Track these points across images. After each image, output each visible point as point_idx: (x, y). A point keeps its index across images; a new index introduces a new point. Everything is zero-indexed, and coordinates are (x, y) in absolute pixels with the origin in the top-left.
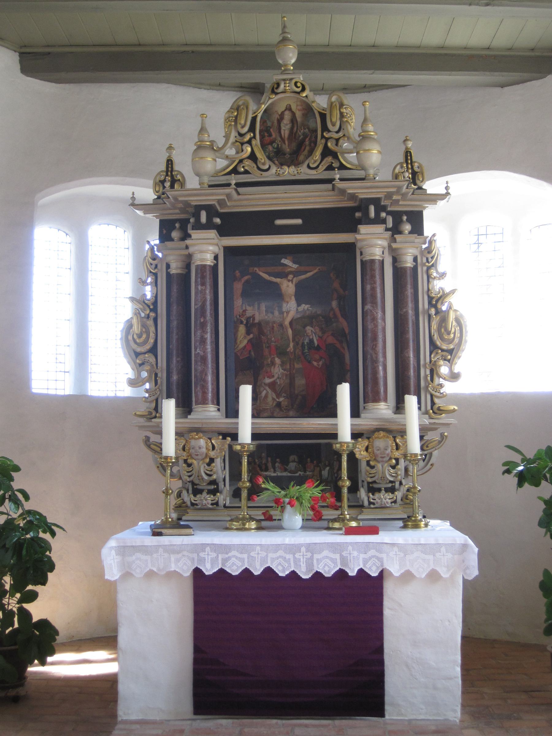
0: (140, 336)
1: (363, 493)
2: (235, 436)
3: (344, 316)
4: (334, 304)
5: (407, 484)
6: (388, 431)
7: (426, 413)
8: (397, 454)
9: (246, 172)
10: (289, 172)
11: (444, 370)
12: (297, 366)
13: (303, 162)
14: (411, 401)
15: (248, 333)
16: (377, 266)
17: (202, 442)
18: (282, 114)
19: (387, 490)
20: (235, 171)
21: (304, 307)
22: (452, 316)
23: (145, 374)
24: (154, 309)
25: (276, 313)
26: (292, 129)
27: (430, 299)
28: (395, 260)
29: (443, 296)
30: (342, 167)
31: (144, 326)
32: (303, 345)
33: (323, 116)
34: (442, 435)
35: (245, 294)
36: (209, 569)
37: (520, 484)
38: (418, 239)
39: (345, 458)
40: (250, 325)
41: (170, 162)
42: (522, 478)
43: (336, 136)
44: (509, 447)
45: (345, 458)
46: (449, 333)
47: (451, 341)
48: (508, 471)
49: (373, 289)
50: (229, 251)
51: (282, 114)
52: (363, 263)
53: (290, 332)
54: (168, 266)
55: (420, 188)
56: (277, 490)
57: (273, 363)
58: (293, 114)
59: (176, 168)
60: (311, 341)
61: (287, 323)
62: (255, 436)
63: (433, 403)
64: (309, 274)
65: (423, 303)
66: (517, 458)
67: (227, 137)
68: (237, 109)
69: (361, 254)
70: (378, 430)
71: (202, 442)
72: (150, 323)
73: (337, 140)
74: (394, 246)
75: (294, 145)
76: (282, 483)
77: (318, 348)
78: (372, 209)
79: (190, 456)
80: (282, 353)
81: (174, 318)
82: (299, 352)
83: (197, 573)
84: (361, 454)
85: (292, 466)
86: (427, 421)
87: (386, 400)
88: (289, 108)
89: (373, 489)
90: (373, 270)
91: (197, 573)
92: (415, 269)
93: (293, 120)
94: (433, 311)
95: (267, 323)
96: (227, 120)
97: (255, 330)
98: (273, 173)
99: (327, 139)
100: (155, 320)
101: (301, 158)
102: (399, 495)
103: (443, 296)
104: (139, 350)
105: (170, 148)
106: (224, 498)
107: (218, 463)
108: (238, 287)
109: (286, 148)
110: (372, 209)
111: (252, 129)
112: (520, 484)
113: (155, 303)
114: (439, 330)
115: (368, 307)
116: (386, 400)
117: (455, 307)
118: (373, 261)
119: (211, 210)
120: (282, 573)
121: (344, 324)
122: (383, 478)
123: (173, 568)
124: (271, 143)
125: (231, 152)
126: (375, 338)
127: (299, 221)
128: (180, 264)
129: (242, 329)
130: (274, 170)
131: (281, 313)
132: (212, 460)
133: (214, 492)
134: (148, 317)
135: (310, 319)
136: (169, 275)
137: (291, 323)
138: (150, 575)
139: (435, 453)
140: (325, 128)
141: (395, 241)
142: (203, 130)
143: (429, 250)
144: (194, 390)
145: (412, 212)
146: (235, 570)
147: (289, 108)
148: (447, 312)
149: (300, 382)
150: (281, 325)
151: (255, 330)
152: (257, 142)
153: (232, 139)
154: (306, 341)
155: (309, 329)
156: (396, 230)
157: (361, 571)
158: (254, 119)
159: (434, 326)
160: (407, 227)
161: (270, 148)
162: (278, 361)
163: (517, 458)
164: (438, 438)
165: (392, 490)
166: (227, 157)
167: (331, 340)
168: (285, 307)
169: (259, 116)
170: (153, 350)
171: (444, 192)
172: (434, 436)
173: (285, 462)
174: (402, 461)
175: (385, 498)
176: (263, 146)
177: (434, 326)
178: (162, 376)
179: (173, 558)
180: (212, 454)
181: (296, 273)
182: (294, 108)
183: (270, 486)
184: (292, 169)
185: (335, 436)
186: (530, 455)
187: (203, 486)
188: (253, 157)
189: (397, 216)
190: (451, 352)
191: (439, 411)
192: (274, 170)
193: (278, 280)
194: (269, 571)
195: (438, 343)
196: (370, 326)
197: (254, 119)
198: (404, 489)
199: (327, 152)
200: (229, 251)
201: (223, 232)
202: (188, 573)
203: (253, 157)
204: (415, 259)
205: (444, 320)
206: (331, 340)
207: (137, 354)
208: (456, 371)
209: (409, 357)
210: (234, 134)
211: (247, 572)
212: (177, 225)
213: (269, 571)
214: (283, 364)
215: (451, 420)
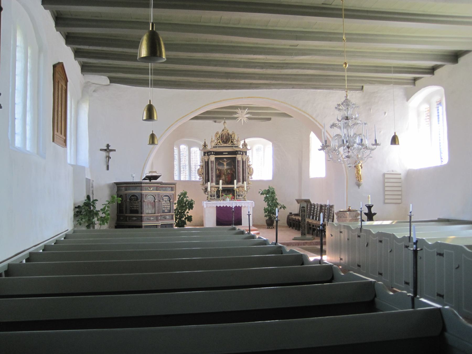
0: (201, 171)
1: (237, 196)
2: (219, 188)
3: (234, 168)
4: (232, 166)
5: (244, 195)
6: (242, 187)
7: (247, 184)
8: (243, 190)
9: (218, 145)
10: (225, 145)
11: (250, 177)
12: (227, 176)
13: (228, 143)
14: (245, 182)
15: (219, 171)
16: (240, 161)
17: (213, 189)
18: (224, 135)
19: (241, 196)
20: (216, 144)
21: (228, 167)
22: (251, 169)
23: (201, 178)
24: (203, 167)
25: (223, 168)
26: (226, 138)
27: (248, 166)
28: (242, 159)
29: (250, 165)
30: (234, 144)
31: (201, 170)
32: (227, 173)
33: (231, 136)
34: (250, 188)
35: (218, 165)
36: (218, 206)
37: (261, 195)
38: (246, 156)
39: (235, 191)
40: (219, 170)
41: (205, 142)
42: (261, 194)
43: (233, 139)
44: (260, 189)
45: (235, 191)
46: (251, 171)
47: (251, 173)
48: (259, 193)
49: (239, 165)
50: (216, 158)
51: (224, 135)
52: (237, 161)
53: (225, 171)
54: (205, 160)
55: (246, 147)
56: (225, 196)
57: (223, 176)
58: (226, 135)
59: (206, 143)
60: (229, 172)
61: (225, 169)
62: (222, 188)
63: (248, 183)
64: (228, 162)
65: (247, 166)
66: (260, 191)
67: (215, 138)
68: (217, 134)
69: (237, 159)
70: (240, 187)
71: (213, 189)
72: (202, 169)
73: (233, 140)
74: (242, 157)
75: (226, 140)
76: (226, 195)
77: (230, 174)
78: (239, 152)
79: (240, 191)
80: (224, 174)
81: (206, 168)
82: (227, 174)
83: (217, 206)
84: (237, 190)
85: (226, 192)
86: (247, 186)
87: (241, 182)
88: (225, 134)
89: (239, 196)
90: (239, 161)
91: (217, 206)
92: (245, 161)
93: (226, 136)
94: (248, 168)
95: (222, 169)
96: (215, 136)
97: (220, 171)
98: (223, 145)
99: (232, 140)
100: (203, 169)
101: (227, 142)
102: (243, 197)
103: (250, 165)
104: (200, 174)
105: (205, 140)
106: (215, 197)
107: (215, 192)
108: (217, 163)
109: (225, 141)
110: (239, 152)
111: (219, 137)
112: (261, 195)
113: (203, 166)
114: (249, 171)
115: (238, 168)
116: (241, 182)
117: (252, 167)
118: (239, 160)
119: (214, 152)
120: (228, 206)
121: (234, 170)
122: (241, 194)
123: (213, 206)
124: (222, 140)
125: (216, 141)
126: (239, 172)
127: (227, 153)
128: (207, 160)
129: (218, 170)
130: (223, 144)
131: (224, 168)
132: (215, 192)
133: (214, 197)
134: (202, 168)
135: (228, 169)
136: (205, 162)
137: (226, 169)
138: (210, 207)
139: (248, 191)
140: (231, 138)
141: (242, 156)
142: (212, 138)
143: (248, 158)
144: (10, 114)
145: (245, 151)
146: (222, 206)
147: (225, 134)
148: (251, 168)
149: (227, 179)
150: (224, 170)
151: (220, 171)
152: (220, 140)
153: (216, 139)
154: (228, 172)
155: (228, 171)
156: (242, 154)
157: (239, 206)
158: (220, 136)
159: (248, 170)
160: (244, 154)
161: (222, 140)
162: (223, 176)
163: (260, 191)
164: (249, 188)
165: (242, 196)
166: (215, 142)
167: (232, 172)
168: (224, 167)
169: (220, 135)
170: (203, 174)
171: (250, 149)
172: (248, 188)
173: (225, 192)
174: (243, 191)
175: (241, 197)
176: (221, 140)
177: (248, 170)
178: (204, 178)
179: (213, 204)
180: (215, 191)
181: (226, 161)
182: (226, 134)
183: (224, 195)
184: (226, 144)
185: (234, 188)
186: (263, 191)
187: (213, 196)
188: (219, 142)
189: (243, 152)
190: (251, 174)
191: (249, 184)
192: (223, 144)
193: (223, 162)
194: (226, 206)
195: (249, 173)
196: (239, 171)
197: (220, 136)
198: (244, 196)
199: (232, 142)
200: (216, 158)
201: (215, 155)
202: (216, 206)
203: (219, 142)
204: (246, 159)
205: (250, 169)
206: (232, 172)
207: (200, 174)
208: (252, 177)
209: (244, 168)
210: (216, 138)
211: (223, 206)
212: (206, 153)
213: (226, 206)
214: (224, 176)
215: (251, 185)
